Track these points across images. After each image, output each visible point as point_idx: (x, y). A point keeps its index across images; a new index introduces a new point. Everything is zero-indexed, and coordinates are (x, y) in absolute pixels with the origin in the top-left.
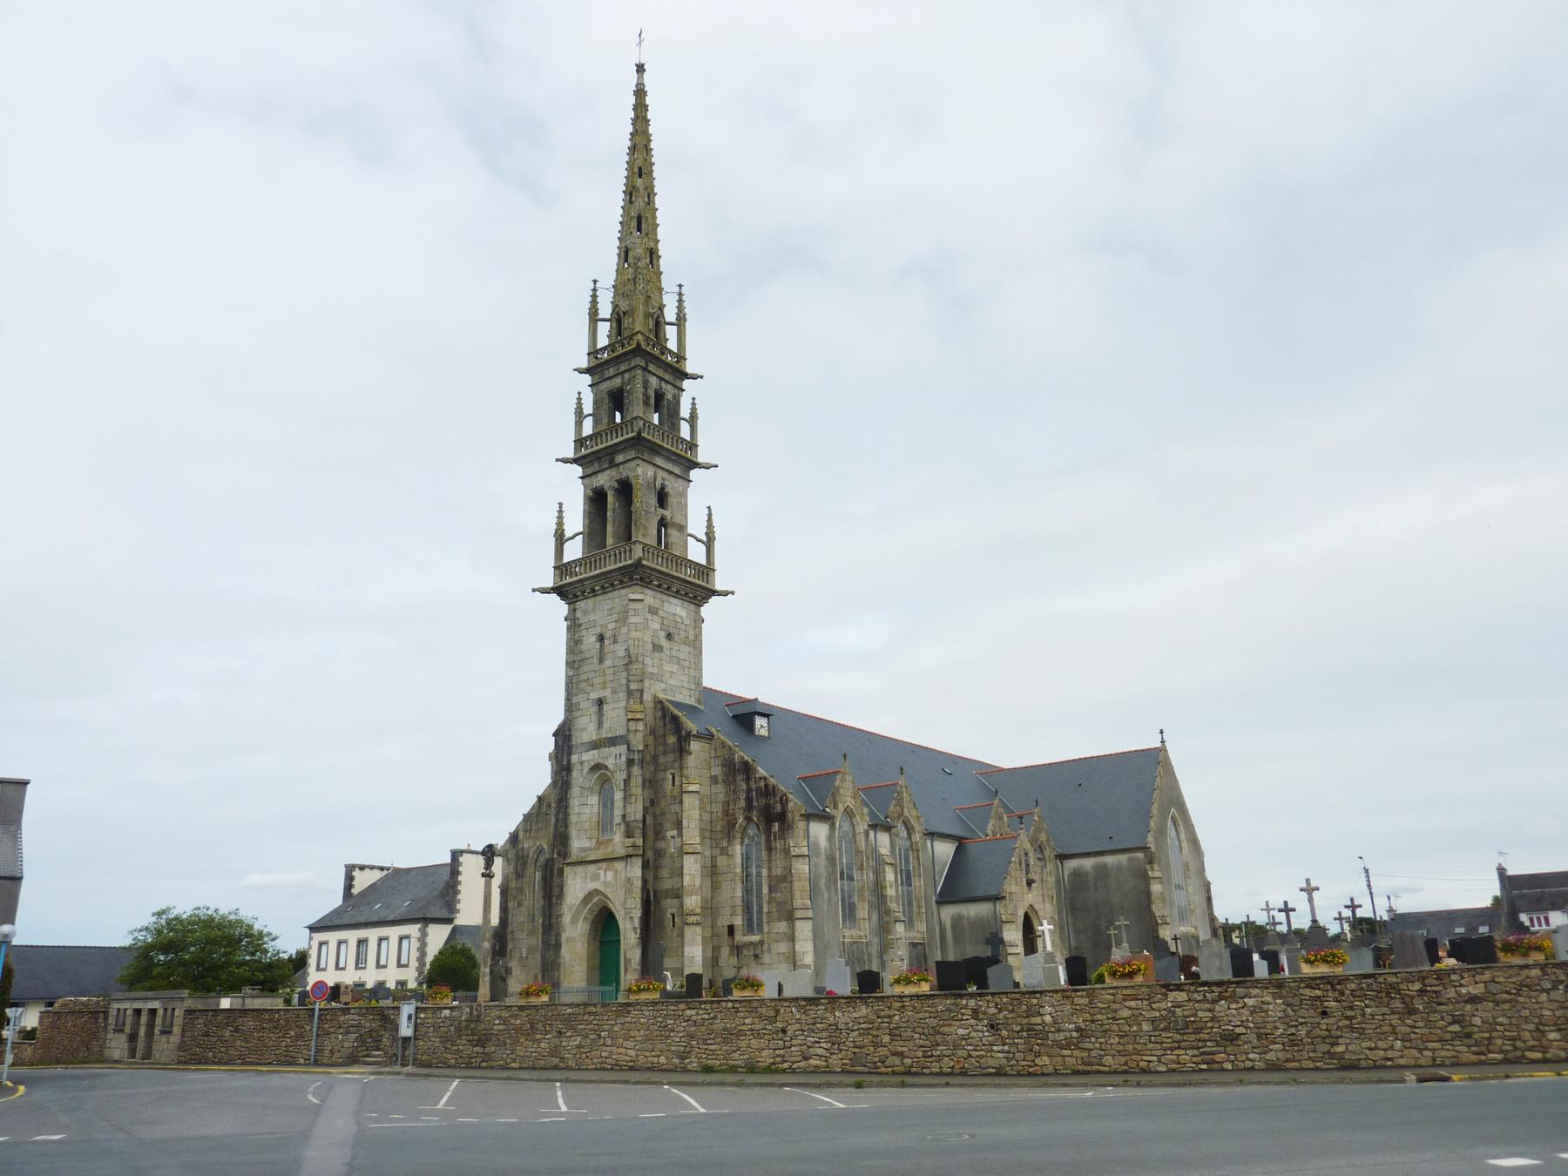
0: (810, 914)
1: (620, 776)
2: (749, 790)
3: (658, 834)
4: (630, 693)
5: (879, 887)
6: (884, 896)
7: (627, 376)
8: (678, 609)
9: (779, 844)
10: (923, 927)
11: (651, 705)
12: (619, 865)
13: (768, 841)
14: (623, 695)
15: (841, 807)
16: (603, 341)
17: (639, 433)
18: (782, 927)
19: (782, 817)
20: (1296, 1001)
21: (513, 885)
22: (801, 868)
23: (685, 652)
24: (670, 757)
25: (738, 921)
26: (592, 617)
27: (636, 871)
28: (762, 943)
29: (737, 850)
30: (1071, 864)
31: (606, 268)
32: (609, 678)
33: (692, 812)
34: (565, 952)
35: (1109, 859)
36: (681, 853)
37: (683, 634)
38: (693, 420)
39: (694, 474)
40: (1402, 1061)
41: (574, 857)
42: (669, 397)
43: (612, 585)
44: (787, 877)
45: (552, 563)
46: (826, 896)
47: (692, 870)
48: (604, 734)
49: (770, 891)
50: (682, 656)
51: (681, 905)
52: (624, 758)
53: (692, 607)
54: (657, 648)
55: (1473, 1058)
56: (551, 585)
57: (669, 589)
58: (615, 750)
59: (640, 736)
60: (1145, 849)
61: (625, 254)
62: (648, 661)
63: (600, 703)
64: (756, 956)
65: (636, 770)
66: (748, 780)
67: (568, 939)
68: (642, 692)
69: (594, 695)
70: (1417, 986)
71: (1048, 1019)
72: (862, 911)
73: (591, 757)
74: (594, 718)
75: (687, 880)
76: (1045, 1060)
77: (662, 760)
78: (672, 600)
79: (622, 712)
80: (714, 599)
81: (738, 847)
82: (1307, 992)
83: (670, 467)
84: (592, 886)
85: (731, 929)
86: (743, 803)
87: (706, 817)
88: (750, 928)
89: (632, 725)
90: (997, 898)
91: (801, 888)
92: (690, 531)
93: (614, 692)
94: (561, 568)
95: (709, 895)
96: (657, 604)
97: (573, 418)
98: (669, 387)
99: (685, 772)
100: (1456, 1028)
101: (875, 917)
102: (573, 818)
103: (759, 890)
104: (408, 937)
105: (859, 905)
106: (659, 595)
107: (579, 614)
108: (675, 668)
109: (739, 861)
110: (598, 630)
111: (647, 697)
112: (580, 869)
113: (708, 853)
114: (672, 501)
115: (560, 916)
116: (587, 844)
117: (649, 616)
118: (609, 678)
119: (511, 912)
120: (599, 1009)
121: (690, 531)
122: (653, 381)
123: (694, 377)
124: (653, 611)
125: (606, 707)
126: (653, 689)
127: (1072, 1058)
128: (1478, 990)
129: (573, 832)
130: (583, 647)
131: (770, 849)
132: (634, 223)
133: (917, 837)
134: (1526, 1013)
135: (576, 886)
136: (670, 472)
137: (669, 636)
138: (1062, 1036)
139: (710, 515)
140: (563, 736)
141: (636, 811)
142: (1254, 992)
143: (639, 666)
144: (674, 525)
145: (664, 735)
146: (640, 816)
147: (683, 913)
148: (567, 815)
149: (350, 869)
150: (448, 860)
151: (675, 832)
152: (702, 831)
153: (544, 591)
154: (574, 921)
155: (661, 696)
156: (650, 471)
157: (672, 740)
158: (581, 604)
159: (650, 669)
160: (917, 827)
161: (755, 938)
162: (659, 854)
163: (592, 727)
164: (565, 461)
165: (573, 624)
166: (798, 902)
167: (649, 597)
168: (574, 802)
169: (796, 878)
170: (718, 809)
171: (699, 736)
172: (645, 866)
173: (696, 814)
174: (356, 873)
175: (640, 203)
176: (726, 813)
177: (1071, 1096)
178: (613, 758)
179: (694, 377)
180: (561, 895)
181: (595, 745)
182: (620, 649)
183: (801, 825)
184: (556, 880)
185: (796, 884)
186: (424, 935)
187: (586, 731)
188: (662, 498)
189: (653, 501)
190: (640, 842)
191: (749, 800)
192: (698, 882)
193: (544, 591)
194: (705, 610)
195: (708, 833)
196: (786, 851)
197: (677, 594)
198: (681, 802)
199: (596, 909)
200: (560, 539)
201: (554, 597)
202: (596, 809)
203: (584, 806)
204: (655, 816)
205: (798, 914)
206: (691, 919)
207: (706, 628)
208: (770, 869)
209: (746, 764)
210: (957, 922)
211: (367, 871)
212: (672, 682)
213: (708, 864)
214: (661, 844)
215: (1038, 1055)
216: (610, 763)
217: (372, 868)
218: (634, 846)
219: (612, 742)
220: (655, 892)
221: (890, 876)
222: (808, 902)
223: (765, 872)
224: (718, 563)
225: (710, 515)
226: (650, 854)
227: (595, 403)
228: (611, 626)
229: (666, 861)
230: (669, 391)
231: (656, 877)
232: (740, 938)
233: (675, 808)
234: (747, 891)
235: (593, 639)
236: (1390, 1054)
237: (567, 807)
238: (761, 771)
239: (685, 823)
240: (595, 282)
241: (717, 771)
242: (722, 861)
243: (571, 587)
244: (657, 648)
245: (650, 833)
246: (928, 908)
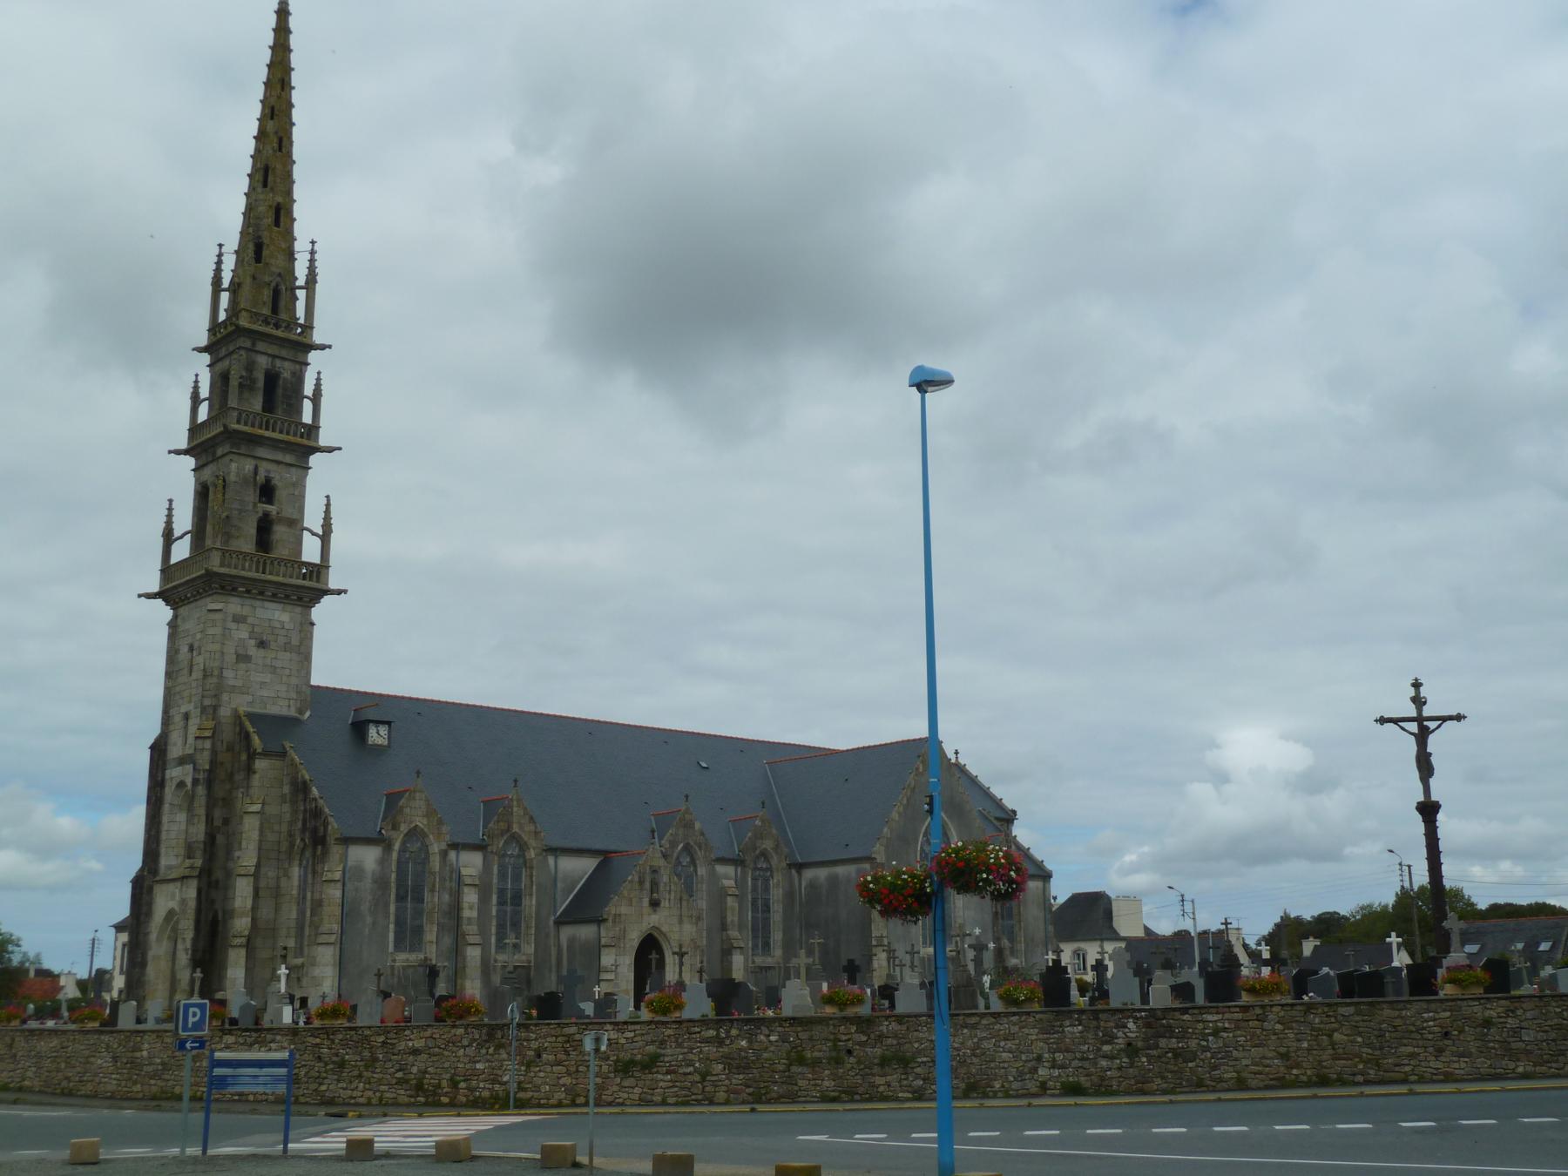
5: (456, 907)
8: (280, 615)
10: (529, 949)
15: (404, 828)
16: (222, 316)
20: (302, 1047)
23: (285, 659)
25: (291, 943)
27: (191, 893)
28: (303, 965)
30: (809, 874)
33: (250, 829)
34: (151, 970)
35: (840, 870)
37: (282, 640)
38: (316, 398)
39: (314, 459)
40: (361, 1100)
42: (286, 375)
45: (158, 565)
50: (279, 664)
53: (298, 610)
54: (243, 658)
55: (406, 1100)
56: (155, 588)
57: (274, 595)
60: (870, 859)
69: (183, 709)
70: (382, 1039)
71: (145, 1053)
76: (138, 1087)
78: (267, 604)
80: (326, 599)
82: (311, 1039)
83: (280, 456)
90: (600, 921)
94: (167, 570)
96: (246, 611)
100: (400, 1075)
102: (164, 836)
106: (248, 602)
108: (268, 678)
109: (296, 883)
114: (281, 494)
115: (147, 934)
123: (323, 347)
124: (239, 619)
127: (155, 1086)
128: (419, 1044)
129: (163, 851)
133: (532, 854)
134: (447, 1065)
138: (150, 1069)
139: (328, 505)
140: (158, 750)
142: (278, 1038)
144: (281, 520)
153: (149, 596)
154: (159, 940)
155: (242, 710)
156: (248, 466)
157: (244, 757)
158: (183, 611)
160: (532, 842)
164: (178, 452)
167: (234, 606)
171: (266, 754)
173: (255, 835)
177: (27, 1114)
179: (323, 347)
187: (175, 751)
193: (149, 596)
197: (274, 598)
200: (169, 537)
201: (160, 602)
207: (317, 632)
209: (305, 782)
210: (572, 941)
212: (265, 693)
215: (135, 1083)
221: (470, 897)
223: (309, 895)
225: (328, 505)
230: (286, 369)
236: (355, 1094)
237: (159, 823)
238: (315, 791)
240: (220, 246)
241: (286, 789)
243: (178, 589)
244: (243, 658)
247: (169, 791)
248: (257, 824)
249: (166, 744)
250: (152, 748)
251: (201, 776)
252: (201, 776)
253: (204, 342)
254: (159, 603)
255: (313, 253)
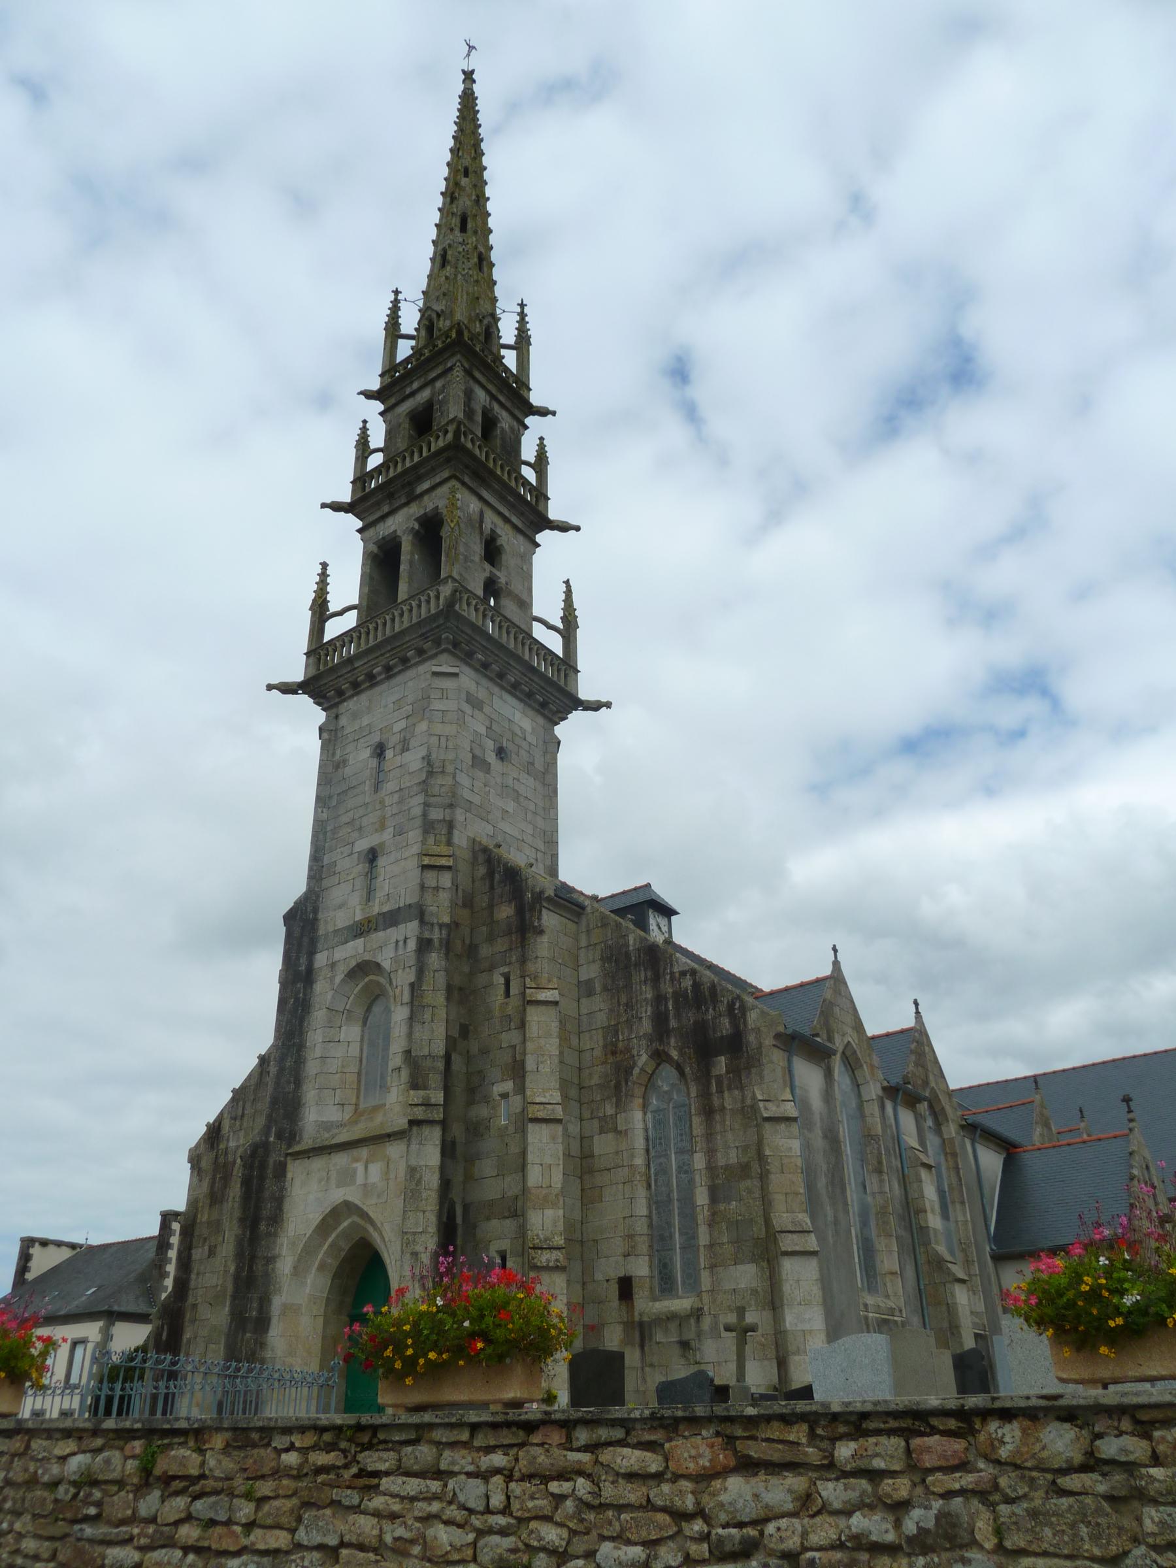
0: (812, 1243)
1: (404, 978)
2: (659, 999)
3: (475, 1091)
4: (428, 827)
5: (911, 1211)
6: (924, 1230)
7: (439, 384)
8: (519, 718)
9: (730, 1100)
11: (467, 855)
12: (395, 1150)
13: (705, 1094)
14: (414, 835)
17: (450, 604)
18: (745, 1276)
19: (735, 1044)
21: (203, 1217)
22: (786, 1145)
24: (501, 945)
26: (365, 721)
27: (431, 1155)
29: (637, 1120)
31: (413, 267)
32: (389, 812)
33: (543, 1037)
36: (524, 1121)
41: (307, 1142)
43: (405, 661)
44: (756, 1165)
45: (303, 646)
46: (829, 1211)
47: (545, 1154)
48: (376, 909)
49: (714, 1198)
50: (522, 790)
51: (522, 1231)
52: (412, 945)
53: (541, 720)
54: (479, 762)
56: (299, 677)
58: (395, 934)
59: (444, 897)
61: (441, 259)
62: (464, 779)
63: (372, 856)
64: (685, 1345)
65: (435, 959)
66: (656, 979)
67: (286, 1307)
68: (451, 825)
69: (363, 845)
72: (889, 1260)
73: (352, 951)
74: (360, 883)
75: (534, 1176)
77: (485, 951)
79: (413, 863)
80: (576, 716)
81: (638, 1115)
84: (338, 1195)
85: (626, 1287)
86: (646, 1026)
87: (571, 1059)
88: (666, 1284)
89: (431, 878)
91: (787, 1187)
92: (536, 612)
93: (400, 832)
94: (318, 649)
95: (577, 1215)
96: (481, 694)
97: (352, 454)
98: (504, 414)
99: (531, 967)
101: (910, 1272)
102: (312, 1067)
103: (688, 1200)
104: (83, 1341)
105: (880, 1244)
107: (343, 721)
108: (511, 806)
109: (639, 1143)
110: (376, 738)
111: (460, 839)
112: (317, 1163)
113: (574, 1129)
114: (508, 559)
115: (271, 1260)
116: (333, 1114)
117: (467, 709)
118: (389, 812)
119: (195, 1267)
120: (217, 1463)
121: (536, 612)
122: (481, 395)
124: (475, 703)
125: (381, 862)
126: (471, 830)
129: (310, 1094)
130: (348, 771)
131: (709, 1112)
132: (456, 222)
135: (309, 1196)
136: (507, 520)
137: (501, 753)
141: (434, 1037)
143: (449, 781)
145: (491, 907)
146: (439, 1048)
147: (526, 1247)
148: (300, 1062)
149: (28, 1243)
150: (154, 1231)
151: (508, 1086)
152: (564, 1085)
153: (287, 689)
154: (298, 1271)
156: (474, 506)
157: (505, 912)
159: (467, 794)
161: (681, 1304)
162: (476, 1130)
163: (355, 900)
165: (329, 735)
166: (782, 1218)
168: (315, 1037)
169: (774, 1166)
170: (594, 1043)
172: (448, 1150)
173: (552, 1046)
174: (36, 1251)
175: (465, 202)
176: (612, 1049)
178: (393, 949)
180: (277, 1218)
181: (361, 930)
182: (414, 759)
183: (777, 1057)
184: (270, 1186)
185: (775, 1179)
186: (107, 1337)
187: (344, 906)
188: (492, 552)
189: (478, 549)
190: (438, 1097)
191: (660, 1020)
192: (557, 1179)
193: (287, 689)
194: (560, 730)
195: (574, 1087)
196: (750, 1114)
197: (513, 688)
198: (522, 1025)
199: (345, 1246)
200: (320, 611)
202: (354, 1050)
203: (335, 1045)
204: (469, 1058)
205: (788, 1243)
206: (544, 1258)
208: (711, 1152)
211: (51, 1248)
213: (575, 1149)
214: (482, 1111)
216: (385, 960)
217: (59, 1244)
218: (427, 1104)
219: (392, 919)
220: (466, 1208)
222: (805, 1220)
224: (583, 661)
226: (457, 1131)
227: (389, 433)
228: (399, 726)
229: (490, 1144)
230: (505, 421)
231: (469, 1178)
232: (646, 1305)
233: (510, 1037)
234: (659, 1204)
235: (366, 754)
237: (301, 1047)
239: (530, 1064)
240: (397, 292)
241: (591, 971)
242: (603, 1145)
244: (479, 762)
245: (459, 1089)
246: (982, 1266)
247: (323, 991)
248: (554, 1025)
249: (315, 911)
250: (290, 918)
251: (436, 935)
252: (436, 935)
253: (375, 385)
254: (304, 701)
255: (522, 315)
